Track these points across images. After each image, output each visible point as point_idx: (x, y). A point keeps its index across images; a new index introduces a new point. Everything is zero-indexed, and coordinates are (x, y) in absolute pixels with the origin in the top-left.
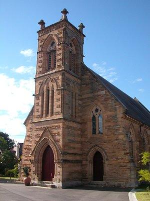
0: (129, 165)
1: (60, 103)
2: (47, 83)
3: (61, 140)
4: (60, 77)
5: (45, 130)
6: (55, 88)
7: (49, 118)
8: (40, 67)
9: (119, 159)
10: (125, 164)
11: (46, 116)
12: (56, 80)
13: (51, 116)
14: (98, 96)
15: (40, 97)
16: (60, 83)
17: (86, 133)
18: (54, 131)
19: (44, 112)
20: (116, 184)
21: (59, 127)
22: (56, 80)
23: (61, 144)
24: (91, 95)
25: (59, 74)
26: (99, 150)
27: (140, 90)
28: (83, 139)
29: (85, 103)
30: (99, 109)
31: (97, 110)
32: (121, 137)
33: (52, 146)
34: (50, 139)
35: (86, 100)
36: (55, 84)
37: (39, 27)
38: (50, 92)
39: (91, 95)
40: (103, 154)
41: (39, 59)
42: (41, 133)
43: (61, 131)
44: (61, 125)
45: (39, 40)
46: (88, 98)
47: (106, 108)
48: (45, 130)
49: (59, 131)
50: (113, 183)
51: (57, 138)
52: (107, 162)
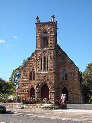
0: (80, 94)
1: (52, 65)
2: (44, 54)
3: (54, 82)
4: (52, 53)
5: (44, 78)
6: (49, 58)
7: (46, 71)
8: (39, 45)
9: (75, 91)
10: (78, 94)
11: (44, 71)
12: (50, 54)
13: (44, 71)
14: (66, 62)
15: (40, 61)
16: (52, 56)
17: (59, 79)
18: (50, 78)
19: (43, 68)
20: (74, 102)
21: (52, 77)
22: (50, 54)
23: (53, 84)
24: (61, 61)
25: (51, 51)
26: (66, 87)
27: (14, 36)
28: (58, 82)
29: (59, 64)
30: (66, 68)
31: (64, 69)
32: (77, 82)
33: (48, 85)
34: (48, 82)
35: (59, 63)
36: (49, 56)
37: (36, 21)
38: (46, 59)
39: (61, 61)
40: (68, 89)
41: (38, 40)
42: (42, 79)
43: (53, 78)
44: (53, 76)
45: (37, 29)
46: (60, 62)
47: (70, 68)
48: (44, 78)
49: (52, 78)
50: (73, 102)
51: (51, 81)
52: (70, 93)
